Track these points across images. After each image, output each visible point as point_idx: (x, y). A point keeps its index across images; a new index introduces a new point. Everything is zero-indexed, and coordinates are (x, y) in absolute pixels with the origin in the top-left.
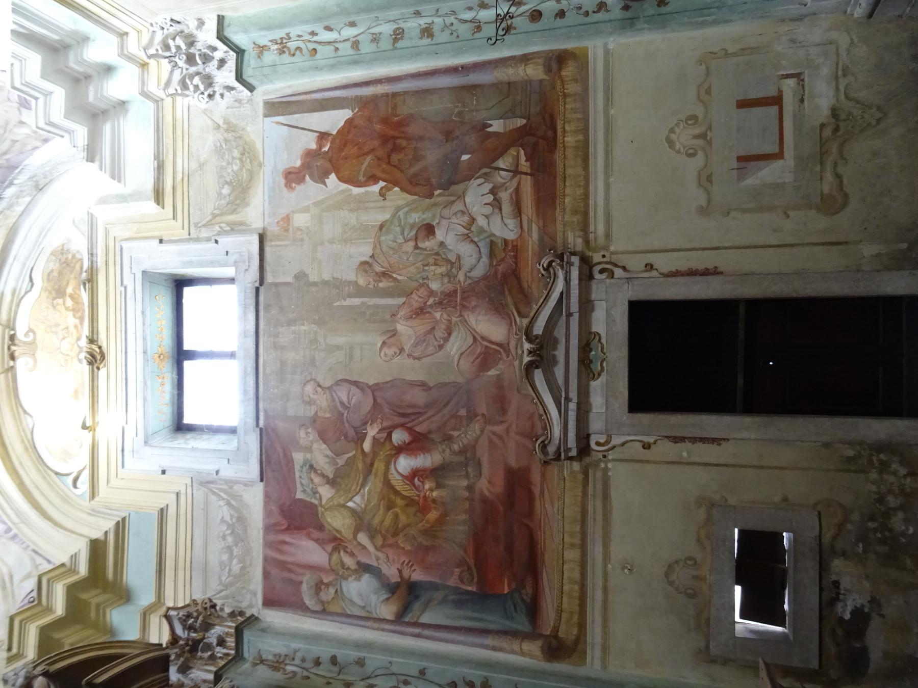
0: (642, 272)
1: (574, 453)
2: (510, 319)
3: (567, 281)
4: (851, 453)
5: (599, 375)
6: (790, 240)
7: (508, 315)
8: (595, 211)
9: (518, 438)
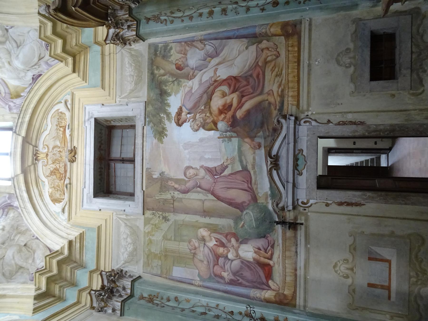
3: (288, 128)
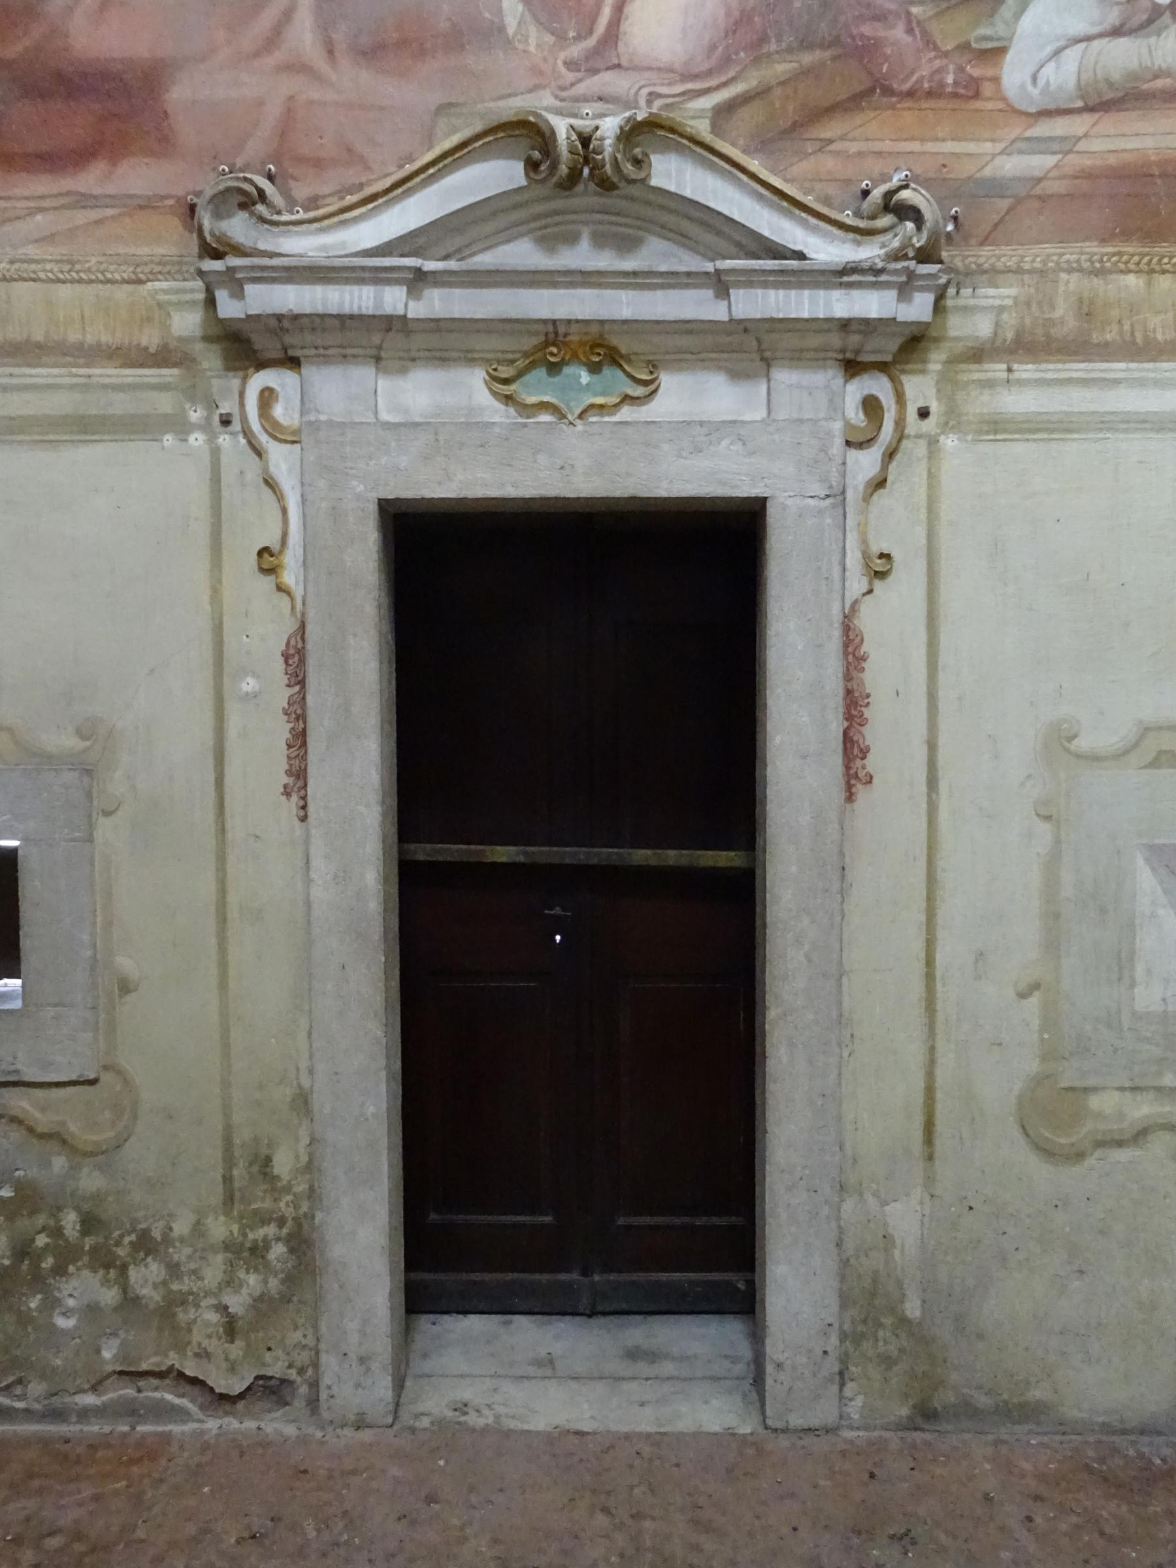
0: (864, 542)
1: (229, 308)
2: (710, 73)
4: (283, 1165)
5: (508, 399)
6: (948, 996)
7: (726, 61)
8: (1085, 382)
9: (273, 111)
